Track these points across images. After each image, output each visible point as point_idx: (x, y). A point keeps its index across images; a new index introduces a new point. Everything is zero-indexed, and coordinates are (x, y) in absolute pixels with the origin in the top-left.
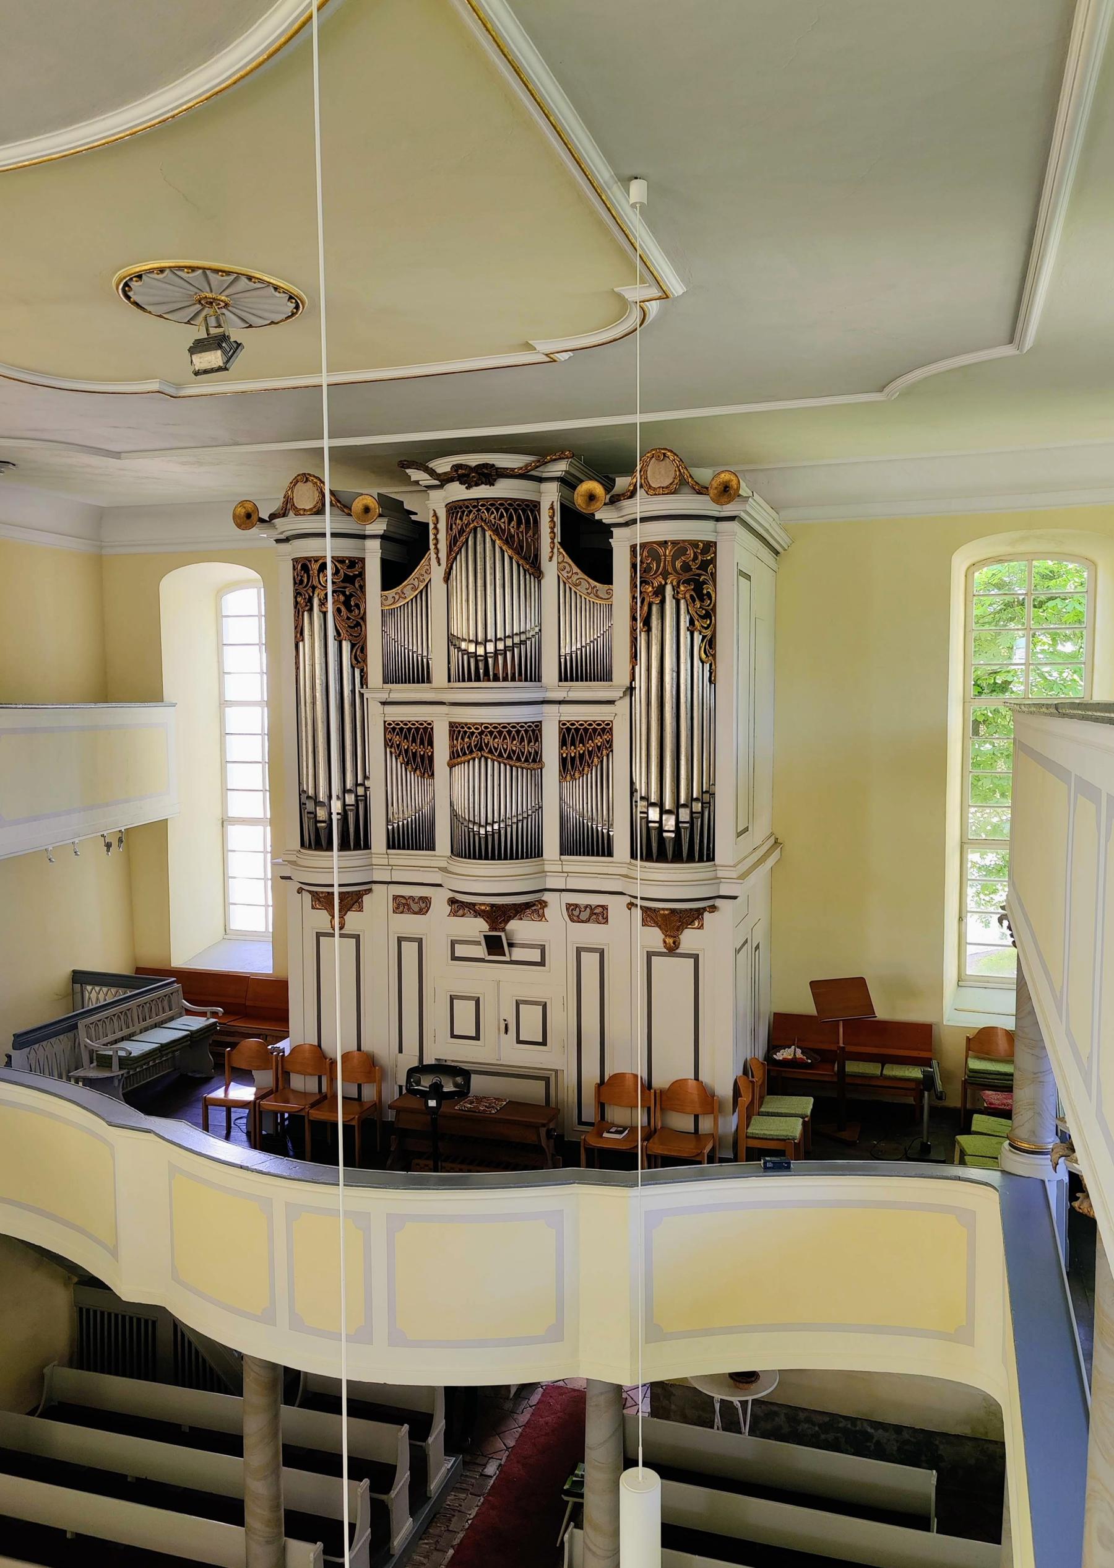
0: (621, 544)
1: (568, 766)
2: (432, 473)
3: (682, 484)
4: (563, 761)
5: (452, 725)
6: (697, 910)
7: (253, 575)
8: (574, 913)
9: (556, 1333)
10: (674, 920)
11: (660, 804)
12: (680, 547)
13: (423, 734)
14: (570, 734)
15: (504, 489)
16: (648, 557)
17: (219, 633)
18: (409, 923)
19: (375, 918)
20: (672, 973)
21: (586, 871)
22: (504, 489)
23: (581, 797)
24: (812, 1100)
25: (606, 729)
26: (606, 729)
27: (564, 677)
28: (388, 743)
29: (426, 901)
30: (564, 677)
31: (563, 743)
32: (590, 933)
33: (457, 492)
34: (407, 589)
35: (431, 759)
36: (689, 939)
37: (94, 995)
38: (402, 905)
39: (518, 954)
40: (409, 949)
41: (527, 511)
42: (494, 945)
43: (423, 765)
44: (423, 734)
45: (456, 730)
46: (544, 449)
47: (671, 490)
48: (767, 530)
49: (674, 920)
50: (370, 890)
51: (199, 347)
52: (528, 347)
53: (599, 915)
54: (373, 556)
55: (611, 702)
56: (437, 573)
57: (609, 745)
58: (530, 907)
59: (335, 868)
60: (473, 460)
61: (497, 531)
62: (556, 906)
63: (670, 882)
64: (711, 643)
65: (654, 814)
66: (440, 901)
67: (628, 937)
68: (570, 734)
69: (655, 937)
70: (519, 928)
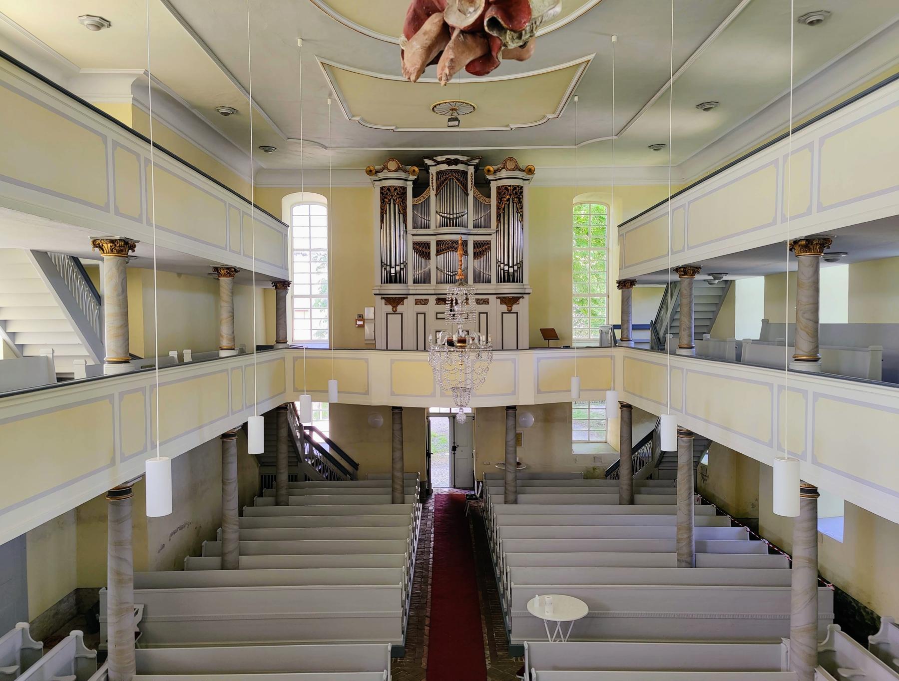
0: (494, 186)
1: (477, 255)
2: (435, 161)
3: (517, 168)
5: (437, 242)
7: (325, 200)
8: (478, 302)
9: (514, 393)
10: (510, 301)
11: (508, 265)
12: (515, 187)
13: (427, 245)
14: (477, 245)
15: (460, 167)
16: (502, 192)
18: (421, 308)
19: (408, 308)
20: (510, 319)
22: (460, 167)
23: (479, 264)
24: (148, 514)
25: (489, 243)
26: (489, 243)
27: (475, 227)
29: (427, 300)
30: (475, 227)
32: (483, 308)
33: (445, 167)
34: (422, 199)
35: (429, 253)
38: (418, 302)
40: (421, 317)
41: (465, 173)
44: (427, 245)
45: (439, 243)
46: (471, 155)
47: (513, 170)
48: (861, 78)
49: (510, 301)
51: (450, 120)
52: (508, 126)
53: (486, 302)
54: (410, 186)
56: (433, 193)
57: (490, 248)
59: (394, 289)
60: (453, 157)
61: (458, 180)
63: (508, 288)
64: (522, 216)
65: (506, 268)
66: (432, 300)
67: (495, 307)
68: (477, 245)
69: (504, 308)
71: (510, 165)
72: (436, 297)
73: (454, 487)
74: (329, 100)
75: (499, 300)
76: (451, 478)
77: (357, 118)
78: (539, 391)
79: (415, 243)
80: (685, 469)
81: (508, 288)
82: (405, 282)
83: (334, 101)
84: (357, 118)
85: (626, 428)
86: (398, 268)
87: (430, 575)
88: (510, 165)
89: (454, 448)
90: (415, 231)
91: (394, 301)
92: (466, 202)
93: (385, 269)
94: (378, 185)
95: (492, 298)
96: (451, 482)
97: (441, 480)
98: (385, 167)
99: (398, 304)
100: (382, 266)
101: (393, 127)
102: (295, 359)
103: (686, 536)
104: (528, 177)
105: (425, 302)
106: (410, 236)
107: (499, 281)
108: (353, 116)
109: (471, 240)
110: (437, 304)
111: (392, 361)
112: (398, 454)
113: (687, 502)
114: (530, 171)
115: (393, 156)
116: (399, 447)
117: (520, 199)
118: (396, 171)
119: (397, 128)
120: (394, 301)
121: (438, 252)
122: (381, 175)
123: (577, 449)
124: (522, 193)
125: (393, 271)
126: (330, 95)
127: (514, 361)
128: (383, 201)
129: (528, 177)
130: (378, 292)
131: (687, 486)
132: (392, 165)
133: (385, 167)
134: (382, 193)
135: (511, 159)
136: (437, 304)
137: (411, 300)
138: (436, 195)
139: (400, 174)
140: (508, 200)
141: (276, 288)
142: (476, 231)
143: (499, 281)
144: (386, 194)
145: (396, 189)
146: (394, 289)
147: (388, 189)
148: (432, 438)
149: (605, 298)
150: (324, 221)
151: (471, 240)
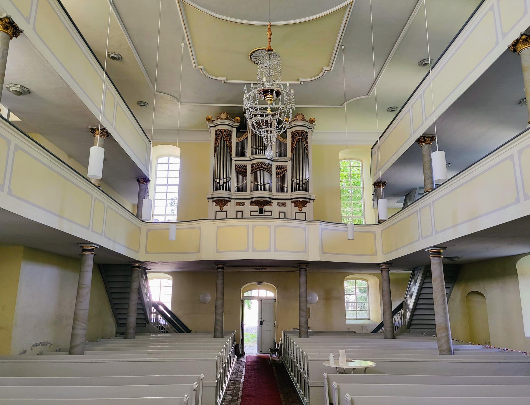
3: (303, 120)
4: (276, 173)
6: (305, 201)
8: (279, 204)
12: (303, 132)
13: (245, 167)
14: (278, 168)
17: (156, 174)
18: (240, 208)
21: (281, 195)
25: (286, 167)
26: (286, 167)
28: (236, 169)
31: (276, 169)
32: (282, 209)
35: (246, 173)
36: (304, 209)
37: (162, 211)
38: (237, 204)
39: (266, 214)
42: (261, 211)
43: (244, 174)
45: (252, 165)
50: (230, 201)
52: (298, 80)
53: (284, 205)
54: (234, 131)
55: (287, 161)
56: (249, 135)
57: (286, 170)
58: (268, 203)
59: (222, 194)
62: (275, 202)
63: (299, 194)
66: (248, 202)
70: (266, 208)
71: (299, 117)
72: (250, 201)
73: (261, 352)
74: (182, 44)
75: (293, 204)
76: (258, 345)
77: (201, 67)
78: (323, 252)
79: (236, 166)
80: (439, 280)
81: (299, 194)
82: (229, 190)
83: (186, 44)
84: (201, 67)
85: (386, 284)
86: (225, 180)
87: (241, 386)
88: (299, 117)
89: (261, 323)
90: (237, 158)
91: (222, 202)
92: (271, 178)
93: (216, 181)
94: (213, 130)
95: (288, 203)
96: (258, 349)
97: (251, 348)
98: (219, 118)
99: (224, 205)
100: (214, 180)
101: (224, 79)
102: (148, 230)
103: (444, 334)
104: (311, 126)
105: (243, 204)
106: (233, 162)
107: (293, 190)
108: (199, 65)
109: (274, 165)
110: (251, 205)
111: (218, 228)
112: (219, 302)
113: (442, 307)
114: (312, 122)
115: (224, 110)
116: (221, 296)
117: (306, 139)
118: (226, 119)
119: (227, 80)
120: (222, 202)
121: (252, 172)
122: (216, 122)
123: (348, 322)
124: (307, 136)
125: (221, 182)
126: (183, 39)
127: (304, 229)
128: (216, 139)
129: (311, 126)
130: (210, 197)
131: (441, 294)
132: (223, 116)
133: (220, 118)
134: (216, 134)
135: (300, 114)
136: (251, 205)
137: (233, 202)
138: (252, 137)
139: (228, 122)
140: (299, 139)
141: (139, 182)
142: (277, 159)
143: (293, 190)
144: (218, 134)
145: (225, 131)
146: (222, 194)
147: (220, 131)
148: (245, 333)
149: (354, 289)
150: (178, 167)
151: (274, 165)
